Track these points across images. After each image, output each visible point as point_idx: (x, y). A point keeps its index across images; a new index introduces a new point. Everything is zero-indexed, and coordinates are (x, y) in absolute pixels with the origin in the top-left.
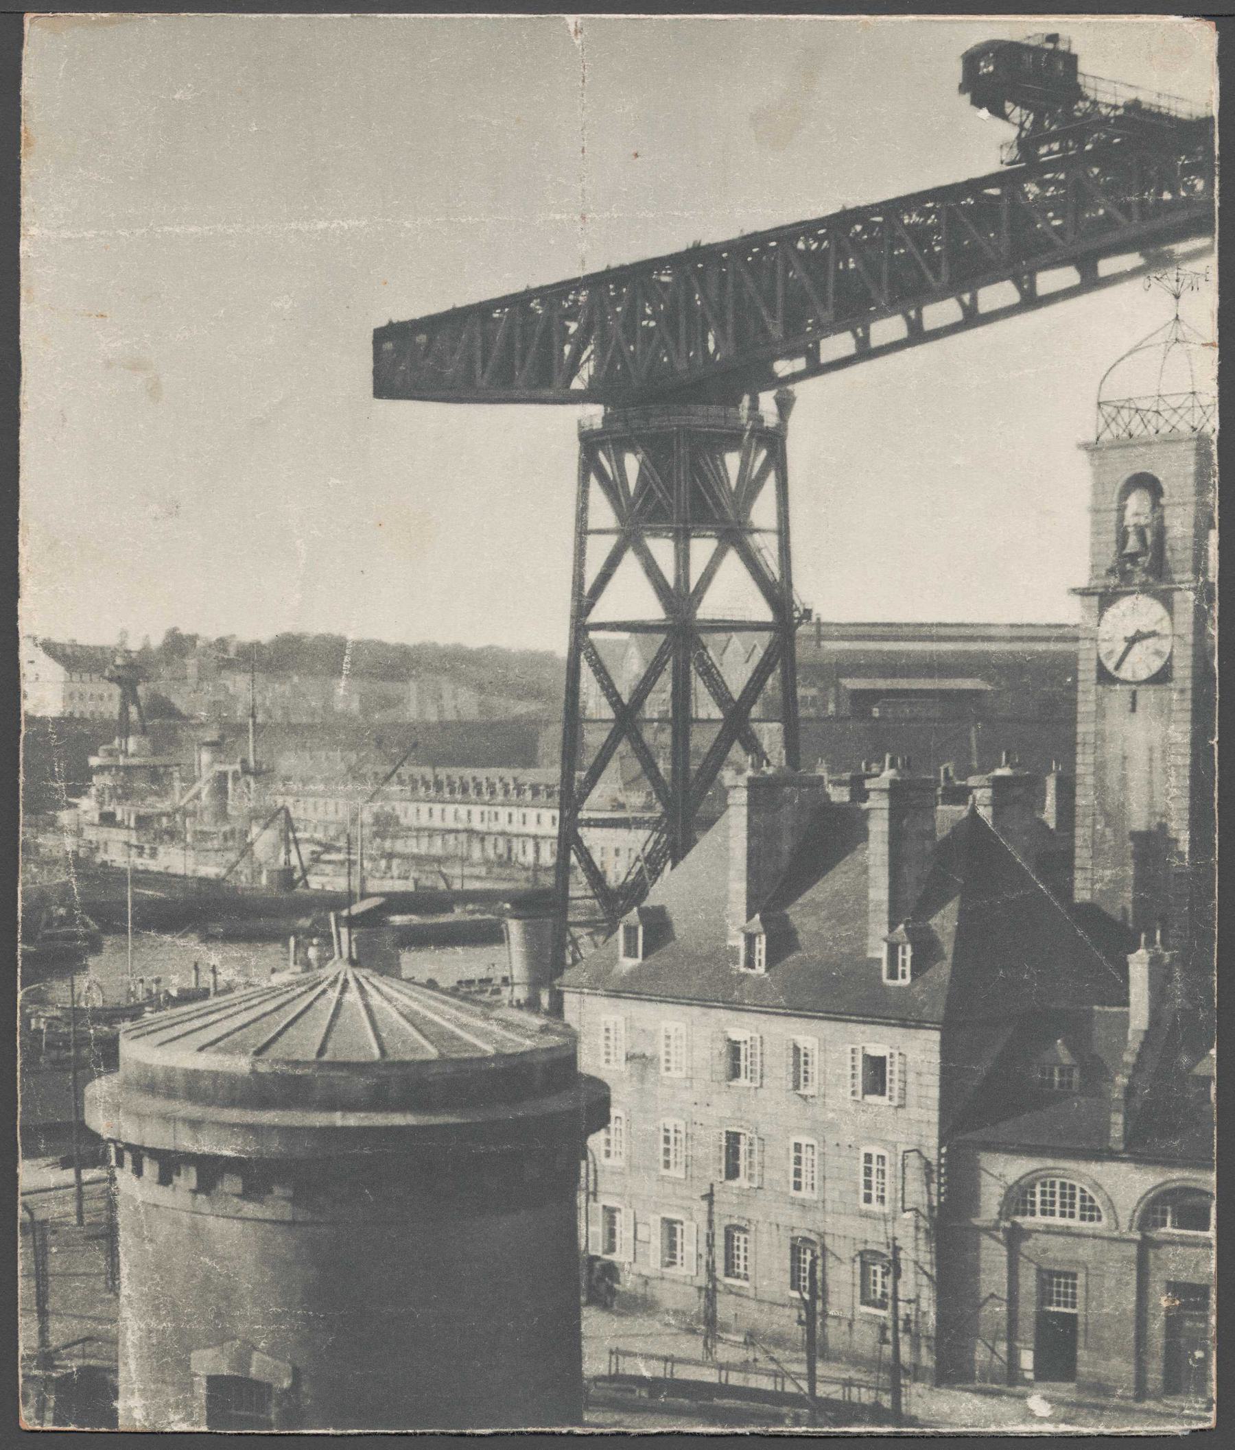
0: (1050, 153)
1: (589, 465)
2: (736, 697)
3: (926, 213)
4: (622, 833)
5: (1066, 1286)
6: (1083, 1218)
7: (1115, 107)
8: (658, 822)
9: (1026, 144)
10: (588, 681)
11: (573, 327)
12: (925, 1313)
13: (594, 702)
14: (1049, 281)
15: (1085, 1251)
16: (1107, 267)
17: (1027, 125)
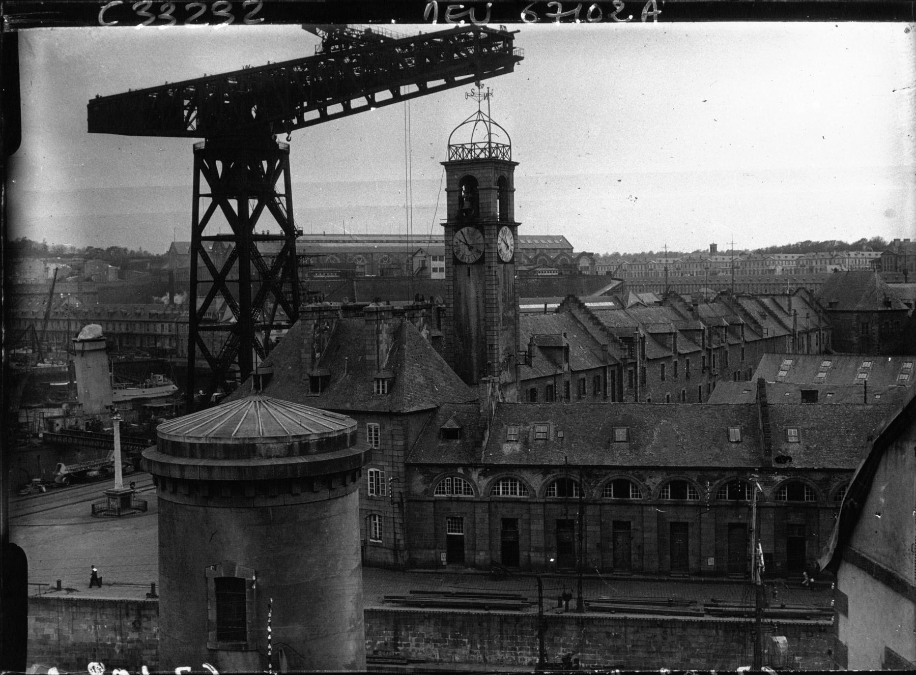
0: (335, 49)
1: (198, 166)
2: (219, 272)
3: (303, 67)
5: (458, 523)
6: (465, 493)
7: (361, 32)
9: (326, 45)
11: (186, 102)
12: (399, 540)
13: (205, 274)
16: (430, 84)
17: (326, 37)
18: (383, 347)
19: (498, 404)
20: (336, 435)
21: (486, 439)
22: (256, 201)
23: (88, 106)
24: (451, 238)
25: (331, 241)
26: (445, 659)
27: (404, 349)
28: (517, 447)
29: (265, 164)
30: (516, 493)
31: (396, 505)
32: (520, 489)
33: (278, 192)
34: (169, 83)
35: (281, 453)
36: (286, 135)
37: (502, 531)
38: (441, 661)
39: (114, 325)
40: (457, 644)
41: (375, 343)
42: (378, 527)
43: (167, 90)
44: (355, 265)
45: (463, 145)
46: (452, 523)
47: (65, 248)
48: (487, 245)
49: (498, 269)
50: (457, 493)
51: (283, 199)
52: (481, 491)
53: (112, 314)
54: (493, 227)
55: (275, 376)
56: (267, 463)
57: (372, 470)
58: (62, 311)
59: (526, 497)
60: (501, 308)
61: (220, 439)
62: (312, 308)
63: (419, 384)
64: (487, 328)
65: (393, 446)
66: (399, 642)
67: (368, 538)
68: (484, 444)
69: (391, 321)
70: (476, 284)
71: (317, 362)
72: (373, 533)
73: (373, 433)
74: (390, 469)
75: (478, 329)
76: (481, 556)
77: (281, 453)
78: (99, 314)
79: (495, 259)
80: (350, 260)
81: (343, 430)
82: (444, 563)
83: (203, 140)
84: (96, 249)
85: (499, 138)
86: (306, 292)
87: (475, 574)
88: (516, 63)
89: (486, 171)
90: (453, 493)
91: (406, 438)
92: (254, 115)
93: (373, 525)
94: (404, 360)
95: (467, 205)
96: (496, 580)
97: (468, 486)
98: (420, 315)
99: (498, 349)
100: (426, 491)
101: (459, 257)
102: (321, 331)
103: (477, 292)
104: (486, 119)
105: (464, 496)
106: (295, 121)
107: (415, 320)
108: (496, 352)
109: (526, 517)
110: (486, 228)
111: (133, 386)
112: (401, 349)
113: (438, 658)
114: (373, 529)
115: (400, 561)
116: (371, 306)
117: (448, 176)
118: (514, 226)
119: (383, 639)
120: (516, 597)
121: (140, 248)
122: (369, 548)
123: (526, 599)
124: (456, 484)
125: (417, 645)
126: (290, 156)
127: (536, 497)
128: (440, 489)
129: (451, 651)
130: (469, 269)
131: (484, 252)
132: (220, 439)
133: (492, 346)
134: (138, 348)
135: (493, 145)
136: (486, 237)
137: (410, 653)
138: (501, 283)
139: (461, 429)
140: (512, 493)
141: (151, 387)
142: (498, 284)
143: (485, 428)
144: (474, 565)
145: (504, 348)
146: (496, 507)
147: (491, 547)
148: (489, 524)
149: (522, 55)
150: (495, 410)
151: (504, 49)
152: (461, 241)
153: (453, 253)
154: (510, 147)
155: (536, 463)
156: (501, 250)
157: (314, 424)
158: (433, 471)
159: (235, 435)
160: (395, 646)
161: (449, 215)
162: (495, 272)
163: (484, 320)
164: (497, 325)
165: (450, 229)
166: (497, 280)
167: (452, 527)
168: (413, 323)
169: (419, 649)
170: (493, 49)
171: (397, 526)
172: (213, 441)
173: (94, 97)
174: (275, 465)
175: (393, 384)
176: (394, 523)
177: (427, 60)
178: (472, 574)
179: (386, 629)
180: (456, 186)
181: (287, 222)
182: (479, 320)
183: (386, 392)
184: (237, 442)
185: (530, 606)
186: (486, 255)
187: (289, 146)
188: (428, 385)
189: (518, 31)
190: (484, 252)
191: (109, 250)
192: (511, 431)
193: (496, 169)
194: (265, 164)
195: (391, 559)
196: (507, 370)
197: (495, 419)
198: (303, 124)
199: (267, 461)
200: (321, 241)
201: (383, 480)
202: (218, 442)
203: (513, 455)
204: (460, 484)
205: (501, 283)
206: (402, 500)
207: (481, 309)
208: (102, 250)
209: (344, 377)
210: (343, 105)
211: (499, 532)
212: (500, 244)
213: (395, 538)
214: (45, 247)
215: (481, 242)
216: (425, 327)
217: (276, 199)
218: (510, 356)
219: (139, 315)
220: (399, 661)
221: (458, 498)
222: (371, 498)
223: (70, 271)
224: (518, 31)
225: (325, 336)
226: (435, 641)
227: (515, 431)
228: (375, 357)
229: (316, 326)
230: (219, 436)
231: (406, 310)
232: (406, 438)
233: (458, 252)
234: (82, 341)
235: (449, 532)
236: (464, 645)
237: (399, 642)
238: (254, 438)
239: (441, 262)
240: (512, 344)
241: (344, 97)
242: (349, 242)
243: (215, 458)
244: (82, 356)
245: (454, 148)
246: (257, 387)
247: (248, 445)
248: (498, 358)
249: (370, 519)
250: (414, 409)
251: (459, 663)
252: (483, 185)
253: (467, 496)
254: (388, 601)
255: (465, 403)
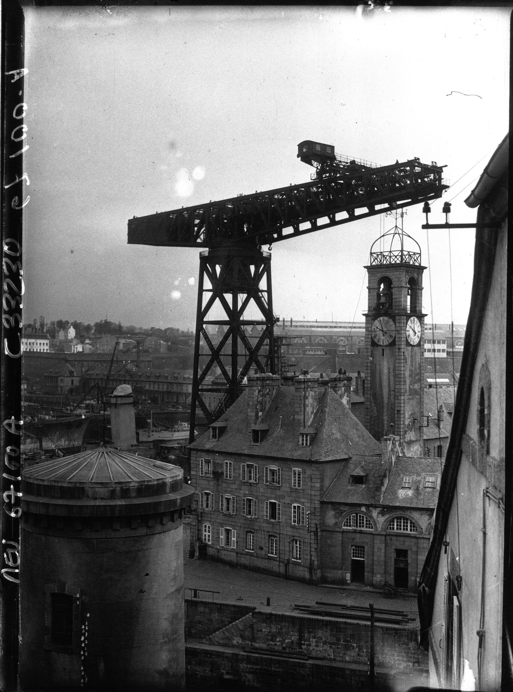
0: (326, 177)
1: (203, 269)
4: (215, 394)
5: (361, 551)
6: (366, 527)
7: (347, 163)
8: (227, 389)
9: (319, 174)
10: (202, 342)
12: (313, 561)
14: (358, 211)
15: (367, 539)
16: (378, 207)
17: (319, 168)
18: (309, 409)
19: (398, 457)
20: (155, 483)
21: (385, 485)
22: (245, 296)
23: (128, 224)
24: (370, 325)
25: (321, 327)
26: (339, 659)
27: (325, 412)
28: (410, 493)
29: (252, 268)
30: (407, 530)
31: (312, 533)
32: (411, 526)
33: (261, 289)
34: (185, 207)
35: (105, 495)
36: (268, 246)
37: (395, 560)
38: (334, 660)
39: (159, 385)
40: (347, 648)
41: (302, 406)
42: (298, 549)
43: (183, 212)
44: (337, 345)
45: (381, 253)
46: (356, 550)
47: (136, 328)
48: (398, 332)
49: (407, 351)
50: (360, 526)
51: (265, 294)
52: (380, 526)
53: (158, 377)
54: (403, 317)
55: (228, 428)
56: (92, 503)
57: (296, 505)
58: (123, 373)
59: (414, 533)
60: (408, 382)
61: (58, 482)
62: (257, 377)
63: (336, 439)
64: (397, 398)
65: (312, 487)
66: (303, 642)
67: (291, 557)
68: (383, 489)
69: (316, 390)
70: (388, 362)
71: (260, 419)
72: (295, 554)
73: (297, 476)
74: (309, 505)
75: (389, 398)
76: (378, 578)
77: (105, 495)
78: (149, 377)
79: (403, 343)
80: (335, 341)
81: (162, 479)
82: (349, 582)
83: (207, 249)
84: (157, 329)
85: (410, 247)
86: (286, 365)
87: (372, 592)
88: (444, 191)
89: (398, 273)
90: (357, 526)
91: (322, 480)
92: (245, 229)
93: (295, 547)
94: (325, 420)
95: (383, 300)
96: (389, 598)
97: (369, 521)
98: (342, 385)
99: (404, 414)
100: (336, 524)
101: (376, 341)
102: (263, 395)
103: (389, 369)
104: (400, 232)
105: (366, 529)
106: (275, 236)
107: (337, 389)
108: (402, 416)
109: (414, 549)
110: (397, 318)
111: (165, 430)
112: (323, 412)
113: (332, 657)
114: (295, 551)
115: (314, 578)
116: (300, 377)
117: (369, 277)
118: (421, 317)
119: (291, 638)
120: (398, 613)
121: (188, 329)
122: (291, 565)
123: (406, 616)
124: (360, 520)
125: (317, 646)
126: (272, 262)
127: (422, 533)
128: (347, 522)
129: (343, 652)
130: (383, 350)
131: (395, 337)
132: (58, 482)
133: (399, 411)
134: (175, 403)
135: (405, 253)
136: (397, 325)
137: (311, 651)
138: (409, 362)
139: (367, 476)
140: (404, 529)
141: (178, 431)
142: (406, 362)
143: (385, 476)
144: (372, 585)
145: (410, 413)
146: (391, 540)
147: (386, 572)
148: (385, 552)
149: (448, 185)
150: (395, 463)
151: (435, 179)
152: (377, 328)
153: (372, 338)
154: (420, 254)
155: (423, 507)
156: (409, 335)
157: (136, 473)
158: (342, 508)
159: (69, 480)
160: (300, 645)
161: (369, 307)
162: (404, 353)
163: (394, 391)
164: (404, 395)
165: (370, 318)
166: (405, 359)
167: (356, 553)
168: (335, 391)
169: (318, 649)
170: (426, 179)
171: (313, 549)
172: (53, 484)
173: (132, 218)
174: (97, 506)
175: (314, 438)
176: (310, 547)
177: (376, 189)
178: (369, 592)
179: (293, 631)
180: (376, 284)
181: (268, 311)
182: (390, 391)
183: (308, 444)
184: (70, 485)
185: (408, 622)
186: (397, 339)
187: (271, 254)
188: (343, 440)
189: (446, 166)
190: (395, 337)
191: (167, 330)
192: (406, 480)
193: (407, 272)
194: (252, 268)
195: (307, 576)
196: (411, 431)
197: (394, 469)
198: (281, 238)
199: (93, 501)
200: (314, 327)
201: (303, 513)
202: (56, 484)
203: (406, 499)
204: (363, 520)
205: (409, 362)
206: (317, 529)
207: (392, 383)
208: (161, 330)
209: (278, 431)
210: (311, 223)
211: (393, 559)
212: (408, 331)
213: (311, 559)
214: (120, 327)
215: (394, 329)
216: (346, 395)
217: (260, 294)
218: (415, 419)
219: (177, 378)
220: (302, 657)
221: (361, 531)
222: (294, 527)
223: (134, 345)
224: (446, 166)
225: (268, 399)
226: (330, 644)
227: (409, 480)
228: (302, 417)
229: (259, 391)
230: (58, 480)
231: (331, 381)
232: (322, 480)
233: (375, 337)
234: (116, 397)
235: (353, 557)
236: (353, 648)
237: (303, 642)
238: (84, 483)
239: (444, 345)
240: (417, 410)
241: (312, 217)
242: (335, 327)
243: (53, 497)
244: (115, 408)
245: (375, 255)
246: (214, 436)
247: (79, 488)
248: (404, 421)
249: (293, 542)
250: (330, 458)
251: (349, 662)
252: (395, 284)
253: (368, 529)
254: (296, 609)
255: (372, 456)
